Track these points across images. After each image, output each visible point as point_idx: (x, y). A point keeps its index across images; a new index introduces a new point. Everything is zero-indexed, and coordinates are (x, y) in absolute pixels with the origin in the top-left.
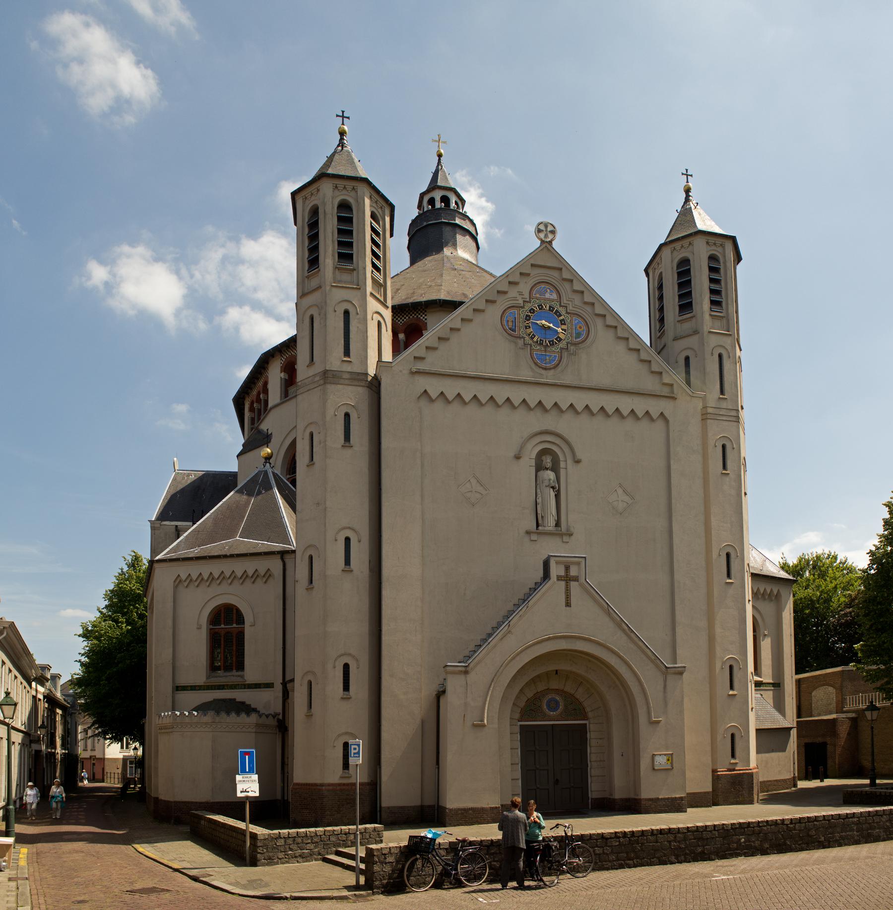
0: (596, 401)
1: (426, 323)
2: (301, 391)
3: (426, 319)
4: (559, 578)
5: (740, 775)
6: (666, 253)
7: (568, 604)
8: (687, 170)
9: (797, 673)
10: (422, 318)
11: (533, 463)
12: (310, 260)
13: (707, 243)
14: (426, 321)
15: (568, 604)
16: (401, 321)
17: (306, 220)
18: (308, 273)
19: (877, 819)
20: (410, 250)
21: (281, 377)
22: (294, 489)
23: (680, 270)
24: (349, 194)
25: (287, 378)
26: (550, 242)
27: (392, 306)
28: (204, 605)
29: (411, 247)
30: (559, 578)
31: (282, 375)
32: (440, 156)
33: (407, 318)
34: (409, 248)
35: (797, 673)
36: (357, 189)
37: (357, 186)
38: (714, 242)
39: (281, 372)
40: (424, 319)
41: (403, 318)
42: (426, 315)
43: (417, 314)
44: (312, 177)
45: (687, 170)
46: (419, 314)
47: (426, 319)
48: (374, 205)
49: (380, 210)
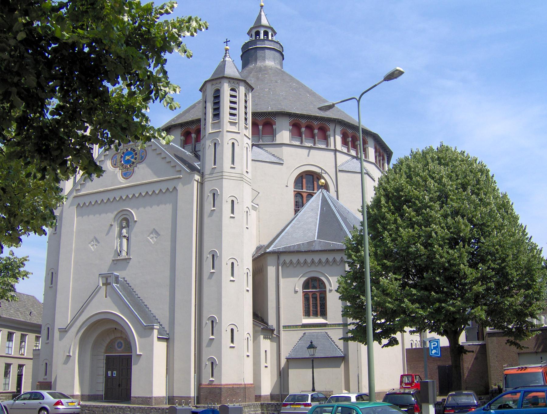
6: (209, 86)
8: (229, 41)
21: (181, 140)
31: (182, 138)
41: (267, 115)
45: (229, 41)
47: (275, 120)
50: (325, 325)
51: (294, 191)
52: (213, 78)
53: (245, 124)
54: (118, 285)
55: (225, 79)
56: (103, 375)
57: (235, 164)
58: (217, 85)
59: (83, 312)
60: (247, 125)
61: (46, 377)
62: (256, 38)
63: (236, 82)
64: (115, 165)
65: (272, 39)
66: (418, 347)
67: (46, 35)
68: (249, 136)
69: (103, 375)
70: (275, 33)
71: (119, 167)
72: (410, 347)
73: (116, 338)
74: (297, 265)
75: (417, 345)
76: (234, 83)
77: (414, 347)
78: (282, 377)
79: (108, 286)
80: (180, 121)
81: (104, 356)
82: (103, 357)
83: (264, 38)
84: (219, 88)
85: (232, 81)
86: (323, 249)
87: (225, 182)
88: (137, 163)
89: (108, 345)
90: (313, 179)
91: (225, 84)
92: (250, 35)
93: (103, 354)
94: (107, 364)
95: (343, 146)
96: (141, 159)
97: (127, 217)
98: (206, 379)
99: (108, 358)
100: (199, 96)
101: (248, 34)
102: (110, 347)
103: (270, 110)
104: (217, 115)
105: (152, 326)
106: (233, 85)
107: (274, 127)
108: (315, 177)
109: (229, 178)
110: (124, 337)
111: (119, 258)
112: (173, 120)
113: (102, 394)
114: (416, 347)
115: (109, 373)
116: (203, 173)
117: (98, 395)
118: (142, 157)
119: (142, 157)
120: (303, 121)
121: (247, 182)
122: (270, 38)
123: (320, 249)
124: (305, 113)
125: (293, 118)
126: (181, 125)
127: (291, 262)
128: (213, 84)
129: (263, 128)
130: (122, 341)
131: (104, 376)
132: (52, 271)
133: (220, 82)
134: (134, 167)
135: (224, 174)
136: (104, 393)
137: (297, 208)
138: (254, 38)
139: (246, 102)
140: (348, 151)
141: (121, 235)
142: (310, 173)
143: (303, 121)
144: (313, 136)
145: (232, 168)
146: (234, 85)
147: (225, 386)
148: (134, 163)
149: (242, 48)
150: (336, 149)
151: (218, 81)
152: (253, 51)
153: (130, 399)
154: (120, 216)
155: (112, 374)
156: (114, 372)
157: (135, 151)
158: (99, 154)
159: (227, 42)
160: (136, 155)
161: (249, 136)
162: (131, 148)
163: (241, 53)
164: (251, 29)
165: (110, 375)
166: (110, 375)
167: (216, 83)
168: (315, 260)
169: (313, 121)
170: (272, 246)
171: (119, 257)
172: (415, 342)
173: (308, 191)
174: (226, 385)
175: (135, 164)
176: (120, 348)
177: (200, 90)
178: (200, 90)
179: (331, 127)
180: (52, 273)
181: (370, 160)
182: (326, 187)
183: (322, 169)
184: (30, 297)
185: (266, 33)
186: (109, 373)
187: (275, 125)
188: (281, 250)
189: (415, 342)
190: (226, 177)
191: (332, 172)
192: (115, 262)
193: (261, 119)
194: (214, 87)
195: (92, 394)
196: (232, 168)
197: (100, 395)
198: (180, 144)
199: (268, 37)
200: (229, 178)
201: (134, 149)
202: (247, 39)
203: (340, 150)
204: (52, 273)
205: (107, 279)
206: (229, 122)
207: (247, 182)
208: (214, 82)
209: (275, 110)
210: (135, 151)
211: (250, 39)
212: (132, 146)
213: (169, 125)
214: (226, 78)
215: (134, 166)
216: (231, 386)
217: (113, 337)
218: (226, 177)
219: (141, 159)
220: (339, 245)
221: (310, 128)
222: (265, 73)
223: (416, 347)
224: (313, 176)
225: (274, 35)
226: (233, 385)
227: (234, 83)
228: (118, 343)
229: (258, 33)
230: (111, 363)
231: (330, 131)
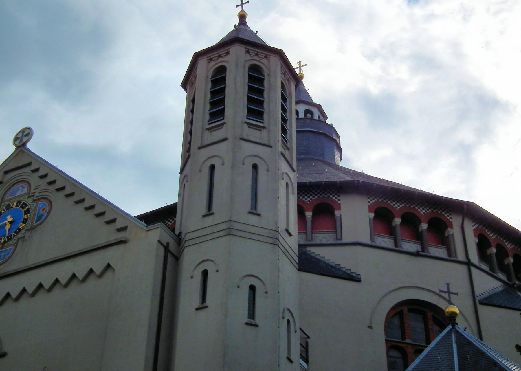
1: (340, 204)
2: (187, 244)
6: (202, 63)
8: (237, 6)
12: (211, 113)
13: (248, 52)
14: (339, 202)
16: (307, 199)
17: (210, 76)
18: (209, 124)
22: (282, 134)
24: (260, 60)
26: (24, 144)
27: (297, 183)
28: (192, 245)
34: (320, 105)
36: (269, 58)
37: (270, 55)
38: (217, 55)
40: (337, 200)
42: (339, 196)
43: (329, 194)
44: (216, 44)
45: (237, 6)
46: (331, 194)
47: (339, 200)
48: (283, 76)
49: (287, 82)
58: (220, 59)
67: (3, 250)
96: (37, 221)
107: (337, 213)
118: (39, 219)
129: (313, 216)
139: (284, 120)
143: (396, 206)
146: (258, 59)
157: (26, 205)
160: (29, 213)
162: (18, 202)
169: (417, 208)
175: (23, 231)
187: (339, 209)
193: (309, 199)
194: (213, 63)
210: (26, 205)
212: (22, 198)
219: (37, 221)
231: (452, 227)
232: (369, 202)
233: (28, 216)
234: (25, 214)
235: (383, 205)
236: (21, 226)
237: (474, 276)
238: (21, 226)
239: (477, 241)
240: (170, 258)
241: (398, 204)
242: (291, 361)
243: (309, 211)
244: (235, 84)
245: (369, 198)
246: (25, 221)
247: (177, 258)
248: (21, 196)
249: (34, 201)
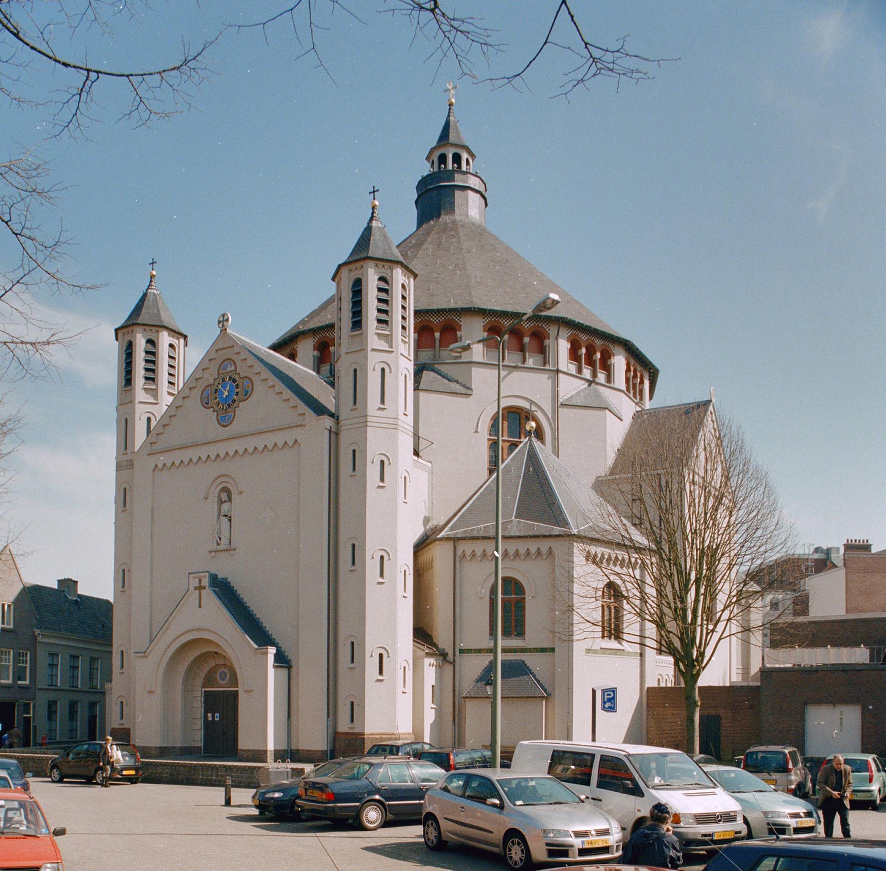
0: (185, 455)
3: (460, 321)
4: (196, 588)
5: (847, 622)
6: (344, 272)
7: (200, 606)
9: (238, 691)
10: (457, 320)
11: (216, 499)
15: (200, 606)
19: (182, 769)
20: (418, 205)
21: (314, 356)
23: (356, 299)
25: (319, 356)
29: (419, 202)
30: (196, 588)
31: (316, 353)
32: (629, 35)
33: (489, 319)
34: (416, 202)
35: (238, 691)
39: (314, 350)
41: (441, 317)
42: (460, 318)
46: (455, 316)
47: (460, 321)
50: (523, 650)
51: (489, 440)
52: (351, 259)
53: (402, 335)
54: (218, 589)
55: (370, 261)
56: (201, 719)
57: (386, 403)
58: (357, 272)
59: (336, 677)
60: (405, 337)
61: (121, 722)
62: (439, 168)
63: (388, 265)
64: (207, 403)
65: (467, 169)
66: (669, 685)
68: (409, 355)
69: (201, 719)
70: (473, 156)
71: (213, 407)
72: (657, 686)
73: (217, 665)
74: (536, 557)
75: (668, 683)
76: (384, 266)
77: (663, 685)
78: (457, 727)
79: (203, 591)
80: (312, 325)
81: (202, 691)
82: (200, 692)
83: (453, 168)
84: (360, 276)
85: (381, 264)
86: (522, 534)
87: (371, 433)
88: (240, 401)
89: (206, 676)
90: (520, 419)
91: (370, 270)
92: (431, 162)
93: (200, 689)
94: (206, 702)
95: (570, 363)
97: (229, 486)
98: (344, 726)
99: (207, 695)
100: (331, 289)
101: (428, 158)
102: (209, 680)
103: (452, 305)
104: (357, 323)
105: (265, 650)
106: (383, 270)
107: (458, 333)
108: (523, 416)
109: (376, 425)
110: (229, 665)
111: (218, 548)
112: (303, 322)
113: (199, 745)
114: (666, 684)
115: (210, 715)
116: (338, 417)
117: (195, 747)
118: (247, 392)
119: (247, 392)
120: (506, 323)
121: (405, 430)
122: (464, 167)
123: (518, 534)
124: (509, 309)
125: (489, 319)
126: (314, 332)
127: (528, 552)
128: (351, 270)
130: (226, 671)
131: (203, 720)
132: (124, 567)
133: (362, 267)
134: (235, 407)
135: (369, 419)
136: (202, 745)
137: (492, 466)
138: (436, 169)
140: (580, 370)
141: (220, 514)
142: (515, 410)
143: (506, 323)
144: (522, 349)
145: (380, 409)
147: (370, 736)
148: (235, 401)
149: (417, 187)
150: (558, 369)
151: (358, 265)
152: (435, 192)
153: (236, 754)
154: (219, 484)
155: (213, 717)
156: (216, 714)
157: (236, 381)
158: (180, 389)
159: (374, 192)
161: (409, 355)
163: (416, 196)
164: (432, 150)
165: (210, 719)
166: (210, 719)
167: (356, 268)
168: (520, 551)
170: (446, 530)
171: (218, 547)
172: (665, 677)
173: (511, 439)
174: (371, 735)
176: (223, 679)
177: (333, 279)
178: (333, 279)
179: (552, 330)
180: (124, 570)
181: (616, 386)
182: (539, 434)
183: (532, 402)
184: (585, 756)
185: (457, 158)
186: (210, 715)
188: (459, 536)
189: (665, 677)
190: (373, 424)
191: (548, 408)
192: (213, 554)
194: (352, 274)
195: (186, 745)
196: (380, 409)
197: (198, 747)
198: (311, 364)
199: (460, 167)
200: (376, 425)
201: (234, 379)
202: (426, 169)
203: (565, 370)
204: (124, 570)
205: (200, 581)
206: (377, 334)
207: (405, 430)
208: (353, 266)
209: (461, 304)
210: (236, 381)
211: (430, 171)
213: (294, 332)
214: (372, 259)
215: (235, 405)
216: (379, 736)
217: (212, 663)
218: (373, 424)
220: (548, 529)
221: (517, 333)
222: (452, 235)
223: (666, 684)
224: (519, 414)
225: (471, 161)
226: (382, 734)
227: (384, 266)
228: (221, 673)
229: (443, 159)
230: (212, 701)
231: (549, 338)
232: (484, 322)
233: (238, 390)
234: (237, 388)
235: (495, 324)
236: (235, 397)
237: (562, 8)
238: (235, 397)
239: (569, 347)
240: (333, 435)
241: (508, 321)
242: (405, 693)
243: (437, 332)
244: (354, 424)
245: (484, 318)
246: (237, 394)
247: (337, 434)
248: (231, 372)
249: (240, 378)
